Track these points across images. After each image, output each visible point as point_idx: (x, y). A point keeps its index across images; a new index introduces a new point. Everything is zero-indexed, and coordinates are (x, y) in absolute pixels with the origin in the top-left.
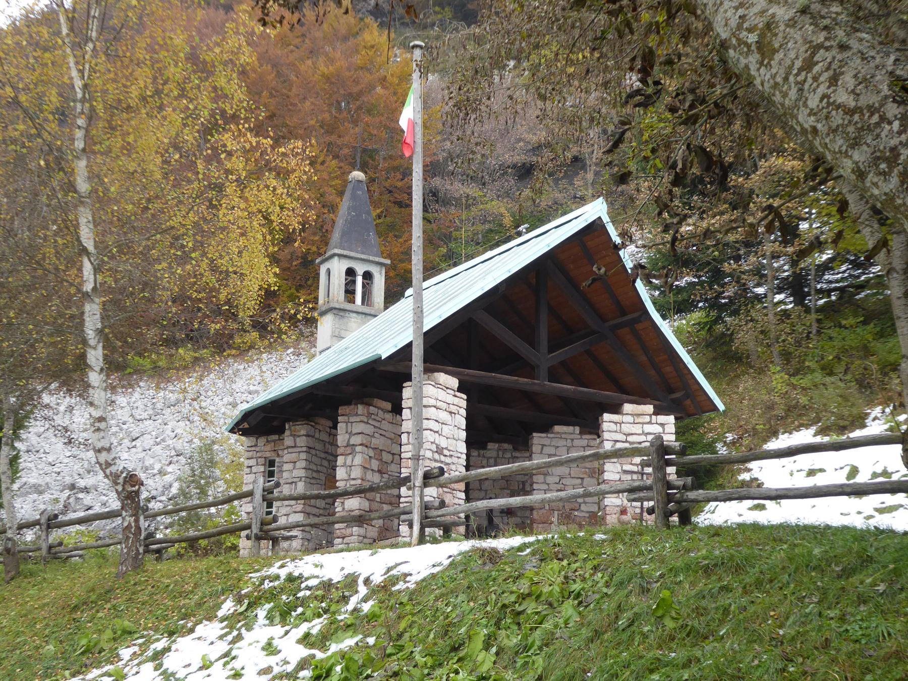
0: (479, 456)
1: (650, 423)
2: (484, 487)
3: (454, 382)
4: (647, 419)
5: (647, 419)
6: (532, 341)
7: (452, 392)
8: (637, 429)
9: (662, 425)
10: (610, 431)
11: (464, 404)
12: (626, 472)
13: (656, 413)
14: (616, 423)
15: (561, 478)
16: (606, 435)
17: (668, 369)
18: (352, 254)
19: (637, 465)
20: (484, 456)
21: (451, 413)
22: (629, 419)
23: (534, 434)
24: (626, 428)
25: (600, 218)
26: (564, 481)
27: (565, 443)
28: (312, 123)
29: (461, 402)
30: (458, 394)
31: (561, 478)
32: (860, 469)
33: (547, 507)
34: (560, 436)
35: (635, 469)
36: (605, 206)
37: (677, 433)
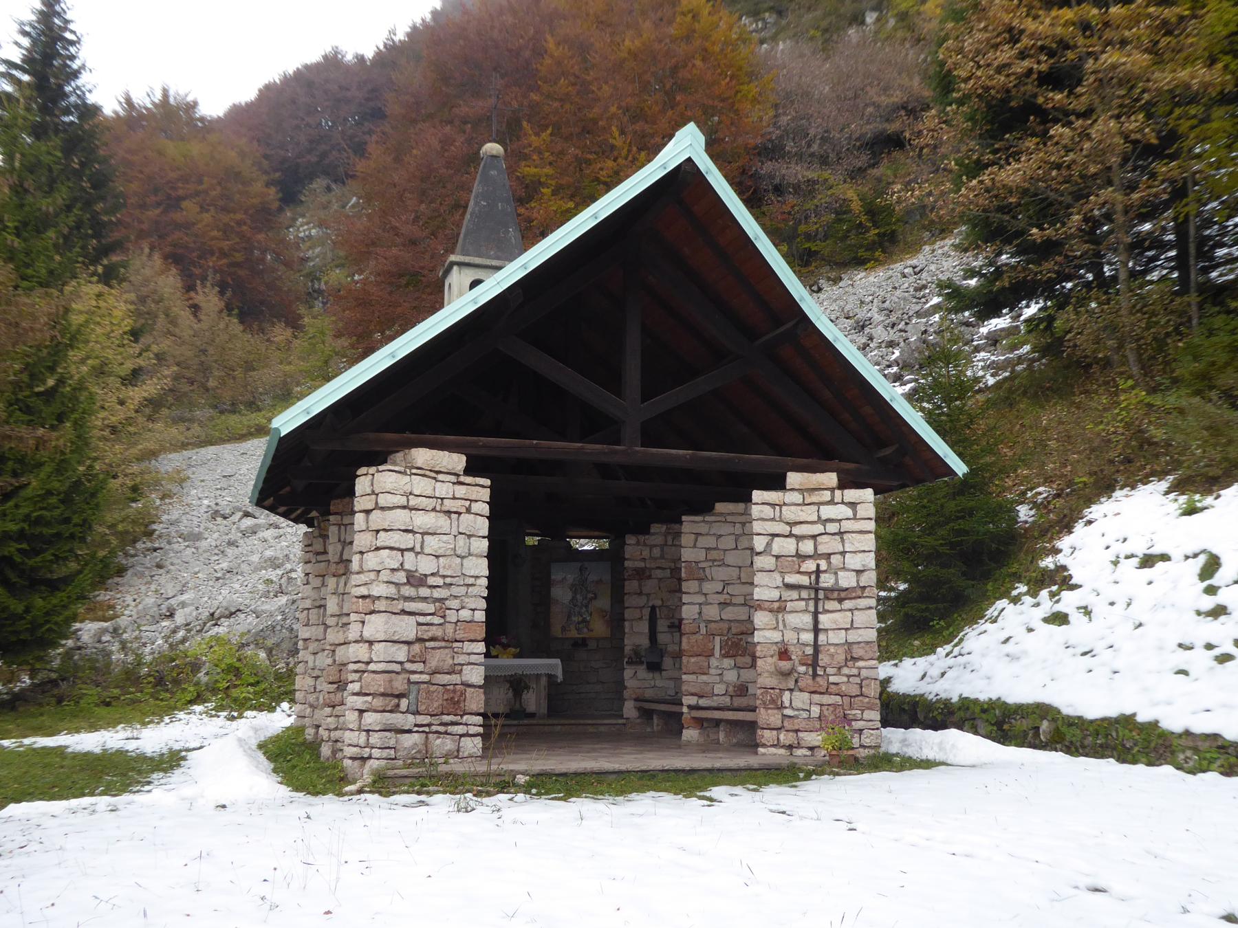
0: (638, 543)
1: (832, 502)
2: (645, 590)
3: (457, 461)
4: (827, 496)
5: (827, 496)
6: (613, 382)
7: (453, 479)
8: (809, 514)
9: (853, 505)
11: (486, 494)
12: (789, 587)
13: (842, 485)
14: (773, 505)
15: (726, 584)
16: (757, 527)
17: (868, 410)
18: (477, 260)
19: (809, 574)
20: (645, 545)
21: (448, 513)
22: (795, 497)
24: (789, 513)
25: (689, 160)
26: (730, 589)
27: (731, 530)
28: (613, 109)
29: (480, 491)
30: (469, 480)
31: (726, 584)
32: (1223, 560)
33: (703, 631)
34: (724, 519)
35: (805, 580)
36: (702, 139)
37: (878, 520)
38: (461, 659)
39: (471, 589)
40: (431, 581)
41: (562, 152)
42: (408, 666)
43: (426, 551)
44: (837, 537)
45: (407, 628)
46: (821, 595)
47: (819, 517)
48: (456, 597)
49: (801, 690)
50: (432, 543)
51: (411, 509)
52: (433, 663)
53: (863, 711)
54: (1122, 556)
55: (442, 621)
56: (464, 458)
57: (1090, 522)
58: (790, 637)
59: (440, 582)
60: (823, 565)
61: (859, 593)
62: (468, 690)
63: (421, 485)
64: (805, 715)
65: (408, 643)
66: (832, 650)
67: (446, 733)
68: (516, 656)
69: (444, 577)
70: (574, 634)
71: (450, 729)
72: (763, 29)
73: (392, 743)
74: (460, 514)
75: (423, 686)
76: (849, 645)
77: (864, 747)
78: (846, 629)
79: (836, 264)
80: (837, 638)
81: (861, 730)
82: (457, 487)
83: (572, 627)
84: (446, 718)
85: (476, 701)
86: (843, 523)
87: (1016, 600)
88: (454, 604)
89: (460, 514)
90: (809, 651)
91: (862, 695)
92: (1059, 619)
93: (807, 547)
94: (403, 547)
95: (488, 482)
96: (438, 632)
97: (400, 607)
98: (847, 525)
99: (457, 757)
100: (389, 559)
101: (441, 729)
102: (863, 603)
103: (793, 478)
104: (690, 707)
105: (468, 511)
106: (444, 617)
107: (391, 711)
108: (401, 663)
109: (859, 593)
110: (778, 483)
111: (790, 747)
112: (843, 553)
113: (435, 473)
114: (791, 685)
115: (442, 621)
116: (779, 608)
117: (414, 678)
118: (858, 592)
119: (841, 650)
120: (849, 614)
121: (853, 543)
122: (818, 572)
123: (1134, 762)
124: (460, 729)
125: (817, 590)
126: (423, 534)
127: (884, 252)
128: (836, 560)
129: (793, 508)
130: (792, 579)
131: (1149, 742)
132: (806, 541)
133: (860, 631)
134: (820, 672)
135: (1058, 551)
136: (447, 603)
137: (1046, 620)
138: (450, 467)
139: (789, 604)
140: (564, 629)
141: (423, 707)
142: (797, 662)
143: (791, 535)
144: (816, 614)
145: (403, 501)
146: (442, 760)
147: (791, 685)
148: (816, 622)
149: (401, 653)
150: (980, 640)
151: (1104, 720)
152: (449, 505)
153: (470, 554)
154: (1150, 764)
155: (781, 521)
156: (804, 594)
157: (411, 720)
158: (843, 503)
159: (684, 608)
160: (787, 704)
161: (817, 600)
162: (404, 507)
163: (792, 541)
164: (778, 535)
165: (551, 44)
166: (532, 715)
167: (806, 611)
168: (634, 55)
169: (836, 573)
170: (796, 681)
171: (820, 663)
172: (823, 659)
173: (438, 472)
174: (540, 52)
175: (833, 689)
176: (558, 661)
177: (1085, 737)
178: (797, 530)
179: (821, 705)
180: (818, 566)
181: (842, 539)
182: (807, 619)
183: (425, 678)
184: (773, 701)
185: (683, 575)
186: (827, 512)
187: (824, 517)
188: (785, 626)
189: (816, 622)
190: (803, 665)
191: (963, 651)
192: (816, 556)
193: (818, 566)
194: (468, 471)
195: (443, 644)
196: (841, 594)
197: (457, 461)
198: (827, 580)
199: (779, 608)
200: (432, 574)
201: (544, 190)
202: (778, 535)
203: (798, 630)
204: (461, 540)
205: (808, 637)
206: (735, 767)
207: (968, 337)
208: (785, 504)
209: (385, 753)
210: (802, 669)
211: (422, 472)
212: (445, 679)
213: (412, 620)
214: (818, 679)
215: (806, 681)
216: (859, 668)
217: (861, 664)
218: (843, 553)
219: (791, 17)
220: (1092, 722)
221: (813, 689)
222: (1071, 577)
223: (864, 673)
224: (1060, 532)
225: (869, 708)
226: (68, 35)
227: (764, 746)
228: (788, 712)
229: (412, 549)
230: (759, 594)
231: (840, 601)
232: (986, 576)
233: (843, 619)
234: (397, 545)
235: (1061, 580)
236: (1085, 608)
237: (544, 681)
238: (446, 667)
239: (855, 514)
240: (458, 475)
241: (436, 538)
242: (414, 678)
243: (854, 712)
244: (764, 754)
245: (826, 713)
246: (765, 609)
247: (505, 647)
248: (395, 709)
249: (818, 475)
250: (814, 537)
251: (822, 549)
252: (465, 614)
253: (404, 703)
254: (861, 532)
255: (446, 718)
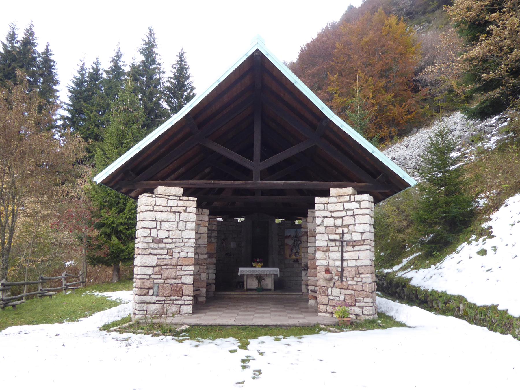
1: (350, 201)
4: (347, 198)
5: (347, 198)
8: (340, 207)
10: (320, 210)
14: (324, 204)
16: (317, 214)
19: (339, 234)
23: (308, 211)
24: (331, 207)
25: (257, 50)
28: (359, 63)
29: (192, 202)
30: (185, 198)
35: (338, 237)
38: (181, 273)
39: (186, 244)
40: (165, 241)
41: (342, 82)
42: (153, 276)
43: (162, 229)
44: (352, 217)
45: (152, 260)
46: (345, 244)
47: (344, 208)
48: (179, 247)
49: (336, 288)
50: (165, 225)
51: (155, 211)
52: (165, 275)
53: (364, 298)
54: (516, 222)
55: (171, 257)
56: (182, 189)
57: (507, 205)
58: (331, 263)
59: (170, 241)
60: (346, 230)
61: (362, 243)
62: (185, 286)
63: (160, 201)
64: (338, 299)
65: (153, 267)
66: (350, 269)
67: (173, 304)
68: (262, 267)
69: (172, 239)
70: (294, 257)
71: (175, 302)
72: (423, 29)
73: (145, 308)
74: (180, 213)
75: (160, 285)
76: (357, 267)
77: (364, 315)
78: (356, 260)
79: (451, 110)
80: (352, 264)
81: (363, 307)
82: (179, 202)
83: (293, 255)
84: (173, 298)
85: (189, 290)
86: (355, 210)
87: (469, 243)
88: (178, 250)
89: (180, 213)
90: (339, 269)
91: (363, 290)
92: (483, 252)
93: (339, 222)
94: (150, 227)
95: (196, 199)
96: (169, 262)
97: (149, 252)
98: (356, 212)
99: (179, 314)
100: (146, 232)
101: (170, 302)
102: (363, 247)
103: (333, 191)
104: (311, 291)
105: (185, 211)
106: (172, 255)
107: (144, 295)
108: (150, 275)
109: (362, 243)
110: (326, 194)
111: (332, 313)
112: (355, 225)
113: (168, 197)
114: (332, 285)
115: (171, 257)
116: (327, 250)
117: (155, 281)
118: (363, 242)
119: (353, 270)
120: (358, 252)
121: (360, 219)
122: (343, 233)
123: (496, 331)
124: (180, 302)
125: (342, 242)
126: (161, 222)
127: (468, 103)
128: (351, 227)
129: (332, 204)
130: (332, 237)
131: (502, 321)
132: (338, 219)
133: (362, 261)
134: (344, 279)
135: (490, 220)
136: (174, 250)
137: (478, 253)
138: (175, 193)
139: (331, 248)
140: (290, 255)
141: (161, 293)
142: (334, 275)
143: (331, 217)
144: (342, 252)
145: (151, 208)
146: (171, 315)
147: (332, 285)
148: (342, 256)
149: (149, 271)
150: (450, 261)
151: (484, 306)
152: (174, 209)
153: (186, 229)
154: (502, 333)
155: (327, 210)
156: (337, 244)
157: (154, 298)
158: (354, 201)
159: (309, 248)
160: (330, 293)
161: (342, 246)
162: (152, 211)
163: (332, 219)
164: (326, 217)
165: (337, 45)
166: (270, 290)
167: (338, 251)
168: (366, 43)
169: (351, 234)
170: (334, 283)
171: (344, 275)
172: (346, 273)
173: (169, 196)
174: (333, 48)
175: (350, 287)
176: (277, 269)
177: (476, 315)
178: (334, 215)
179: (345, 295)
180: (343, 230)
181: (354, 218)
182: (339, 255)
183: (162, 281)
184: (324, 292)
185: (308, 235)
186: (348, 206)
187: (346, 208)
188: (329, 258)
189: (342, 256)
190: (337, 276)
191: (442, 267)
192: (342, 226)
193: (343, 230)
194: (184, 195)
195: (171, 267)
196: (353, 244)
197: (179, 191)
198: (347, 237)
199: (327, 250)
200: (166, 238)
201: (335, 95)
202: (326, 217)
203: (335, 260)
204: (181, 224)
205: (339, 263)
206: (288, 325)
207: (490, 131)
208: (329, 203)
209: (141, 312)
210: (336, 278)
211: (161, 196)
212: (173, 281)
213: (155, 256)
214: (344, 283)
215: (338, 283)
216: (362, 278)
217: (362, 276)
218: (355, 225)
219: (433, 22)
220: (479, 307)
221: (341, 287)
222: (492, 232)
223: (364, 280)
224: (494, 210)
225: (366, 297)
226: (186, 67)
227: (320, 312)
228: (330, 297)
229: (156, 228)
230: (318, 244)
231: (353, 246)
232: (460, 231)
233: (355, 255)
234: (147, 227)
235: (488, 233)
236: (495, 247)
237: (273, 276)
238: (172, 277)
239: (360, 207)
240: (180, 197)
241: (168, 223)
242: (155, 281)
243: (359, 298)
244: (320, 316)
245: (347, 298)
246: (321, 251)
247: (258, 263)
248: (147, 294)
249: (343, 189)
250: (342, 217)
251: (345, 223)
252: (183, 254)
253: (151, 292)
254: (363, 214)
255: (173, 298)
